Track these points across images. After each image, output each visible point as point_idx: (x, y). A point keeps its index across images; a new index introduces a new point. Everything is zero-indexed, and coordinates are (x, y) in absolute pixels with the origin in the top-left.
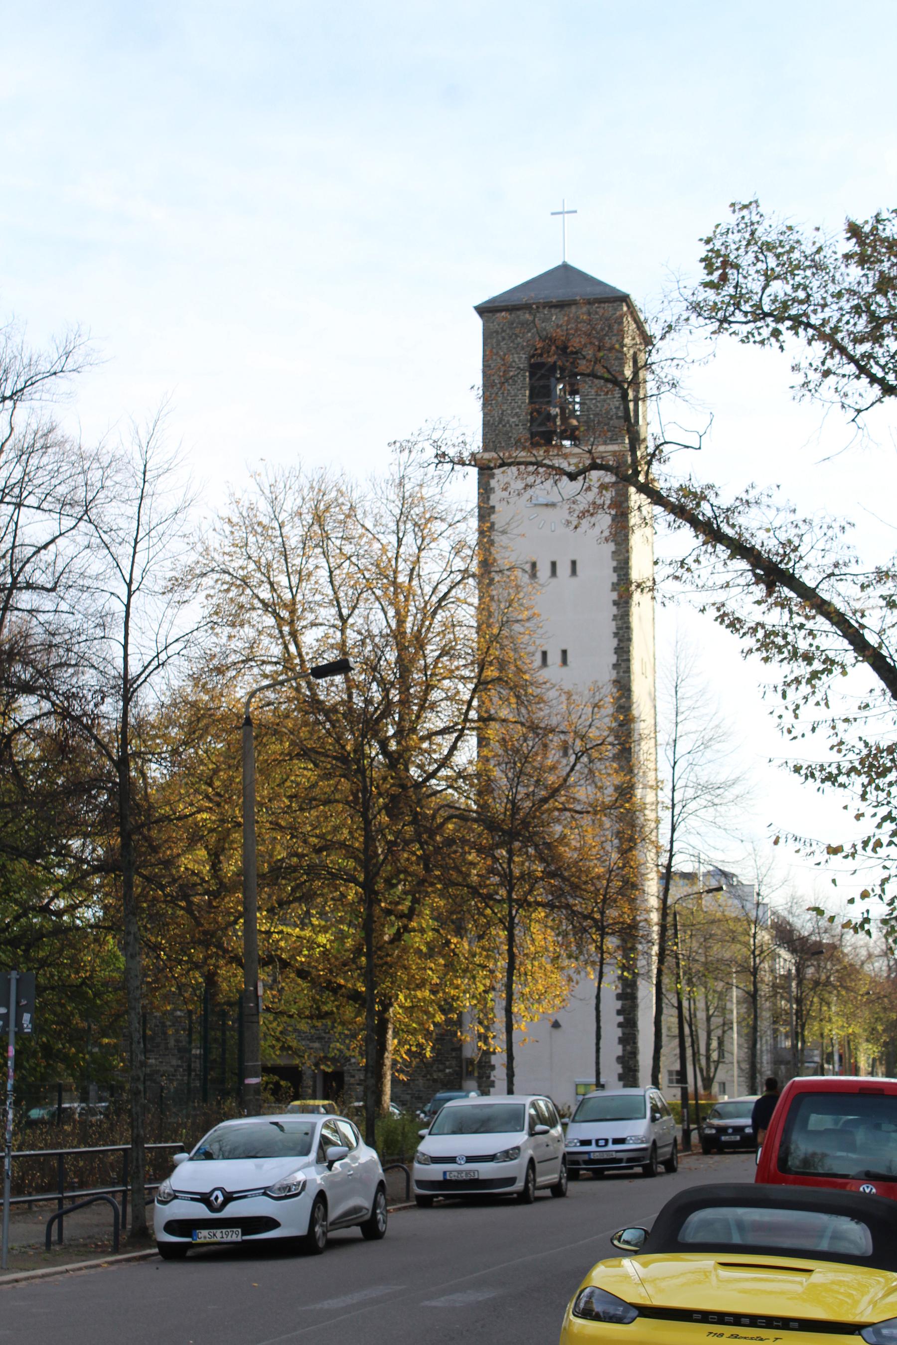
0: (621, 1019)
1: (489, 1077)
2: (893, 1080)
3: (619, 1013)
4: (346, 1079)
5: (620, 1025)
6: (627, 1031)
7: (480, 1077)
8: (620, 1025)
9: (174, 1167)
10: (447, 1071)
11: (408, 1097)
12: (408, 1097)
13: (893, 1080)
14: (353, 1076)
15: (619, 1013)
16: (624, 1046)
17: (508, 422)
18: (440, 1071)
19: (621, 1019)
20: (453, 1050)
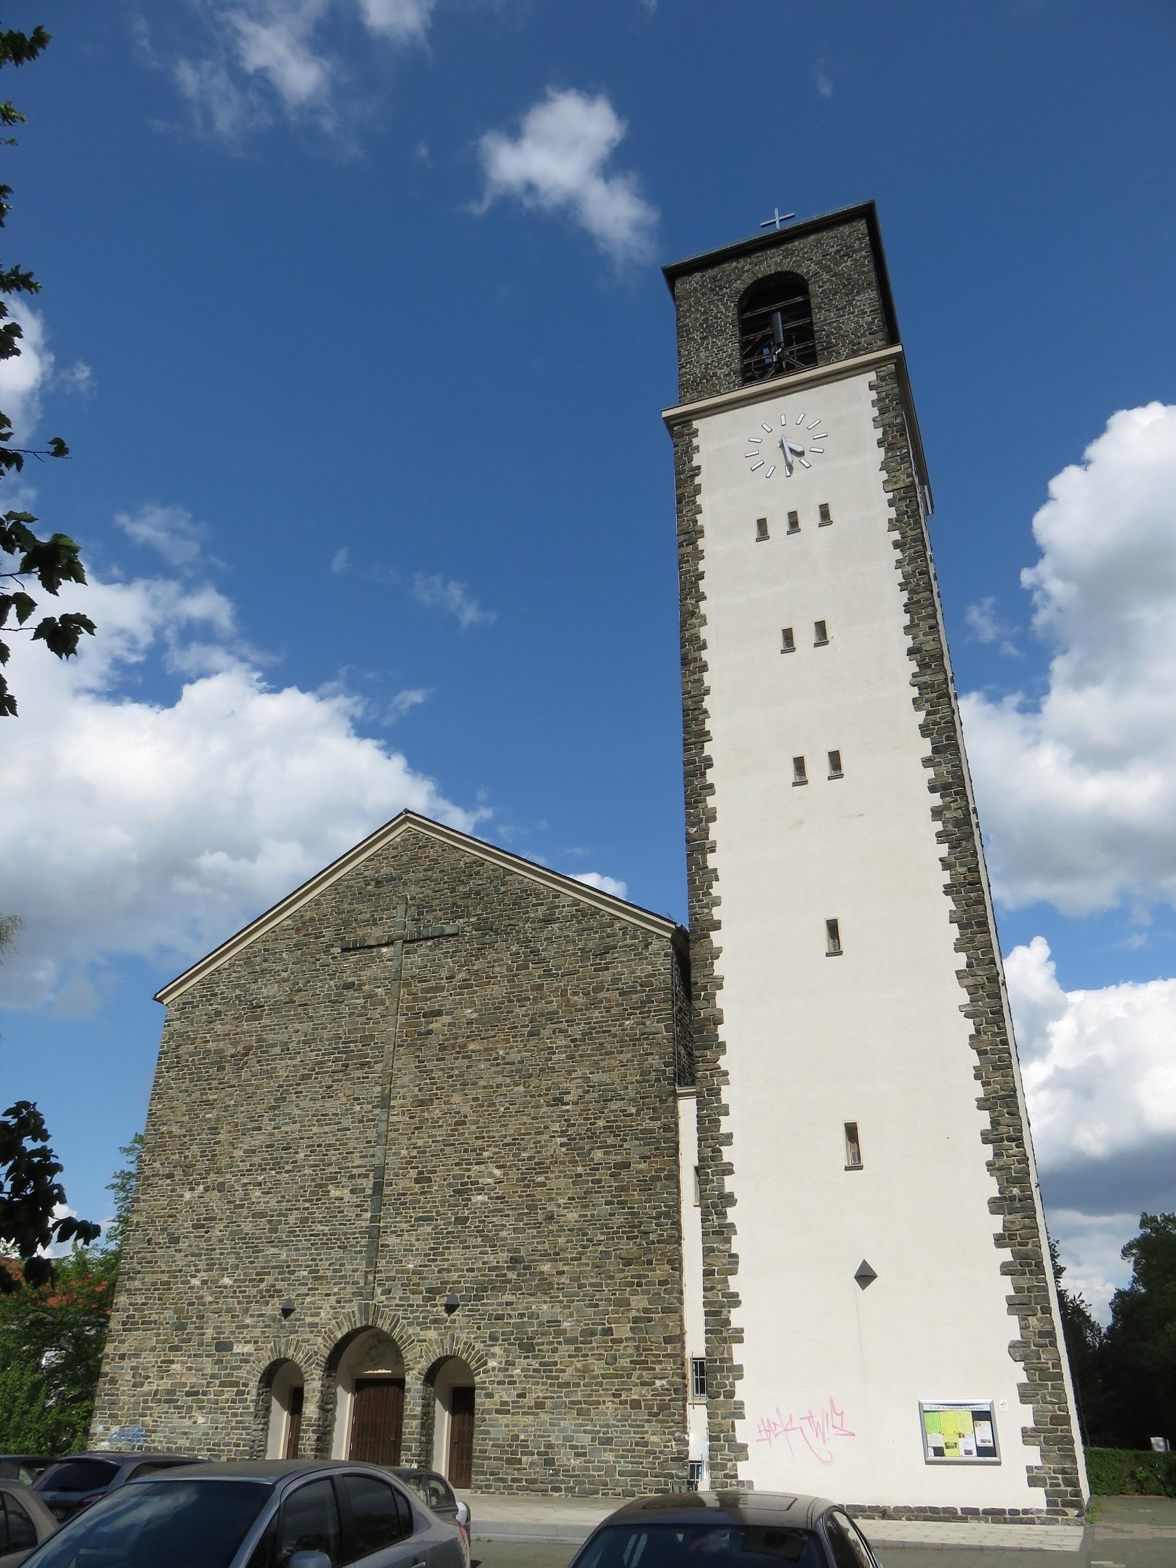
0: (1006, 1255)
1: (731, 1394)
2: (1167, 1533)
3: (1000, 1241)
4: (478, 1400)
5: (1006, 1269)
6: (1024, 1282)
7: (1022, 1179)
8: (1006, 1269)
9: (11, 551)
10: (658, 1383)
11: (586, 1439)
12: (586, 1439)
13: (1167, 1533)
14: (490, 1396)
15: (1000, 1241)
16: (1023, 1319)
17: (715, 374)
18: (643, 1384)
19: (1006, 1255)
20: (668, 1340)
